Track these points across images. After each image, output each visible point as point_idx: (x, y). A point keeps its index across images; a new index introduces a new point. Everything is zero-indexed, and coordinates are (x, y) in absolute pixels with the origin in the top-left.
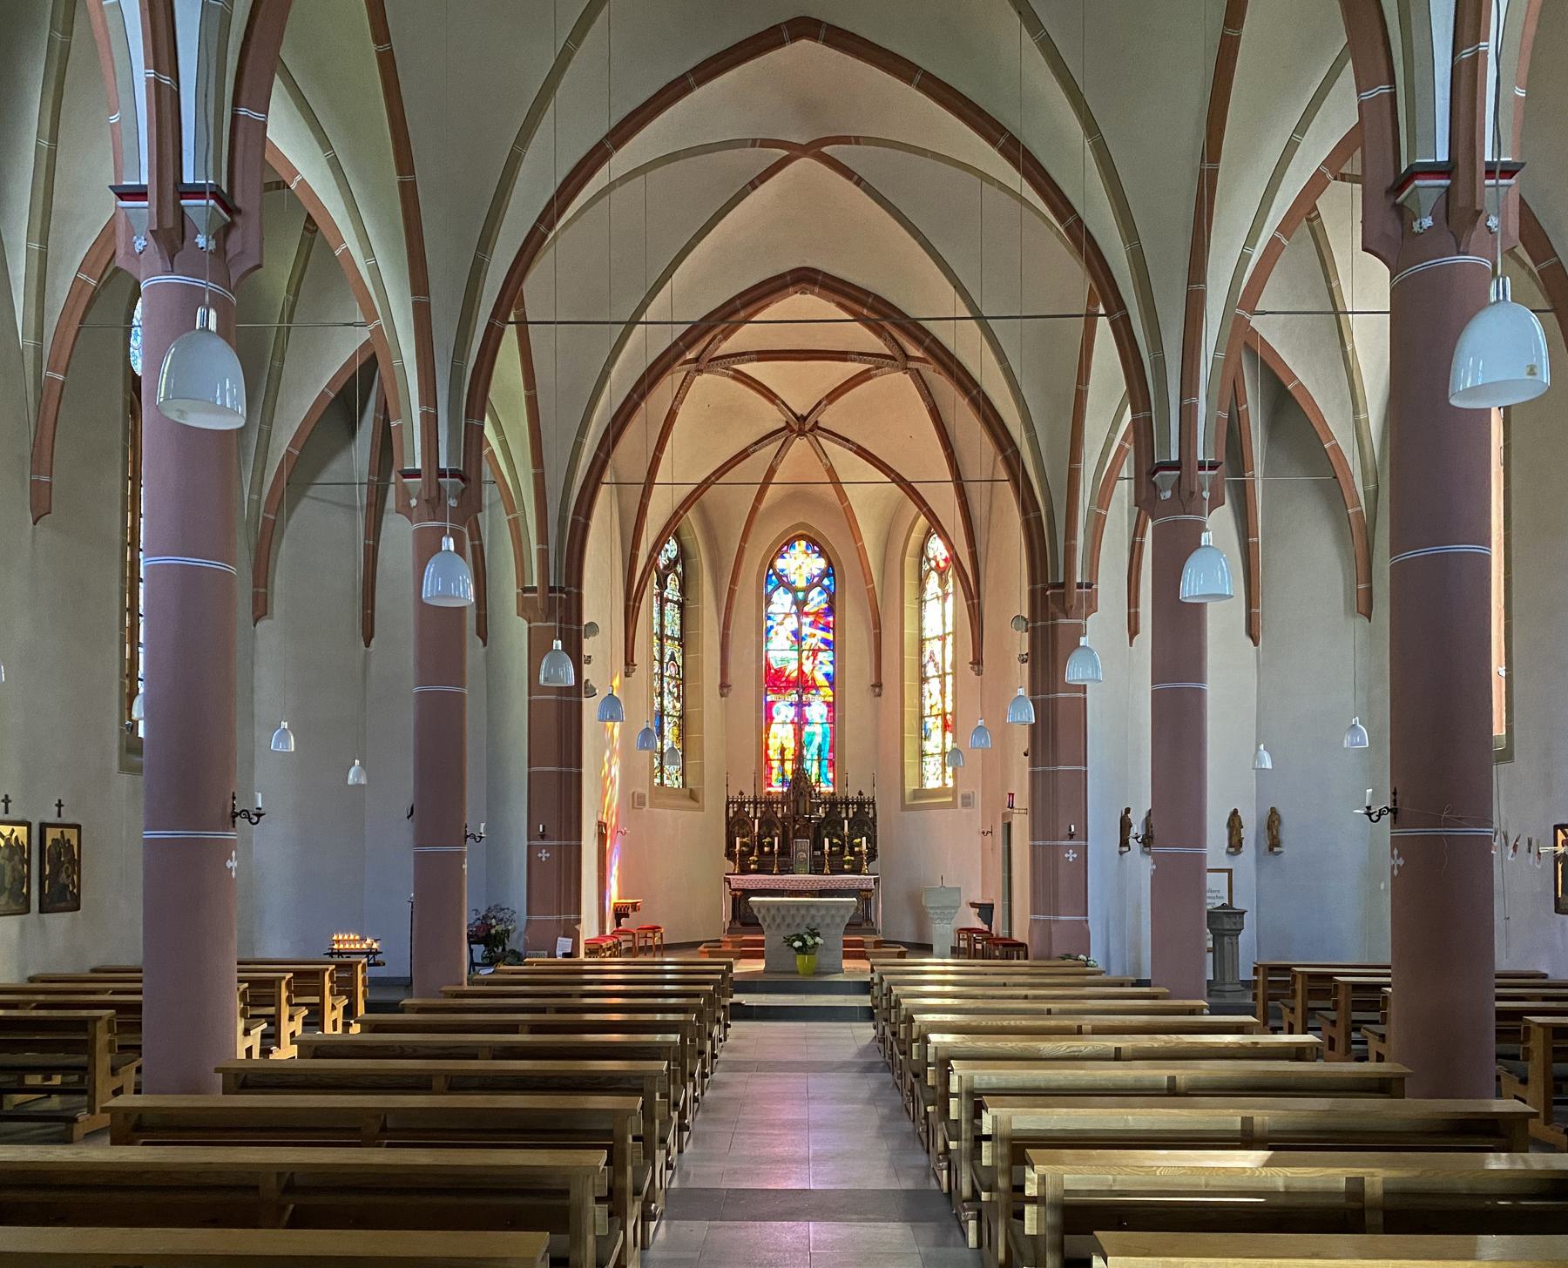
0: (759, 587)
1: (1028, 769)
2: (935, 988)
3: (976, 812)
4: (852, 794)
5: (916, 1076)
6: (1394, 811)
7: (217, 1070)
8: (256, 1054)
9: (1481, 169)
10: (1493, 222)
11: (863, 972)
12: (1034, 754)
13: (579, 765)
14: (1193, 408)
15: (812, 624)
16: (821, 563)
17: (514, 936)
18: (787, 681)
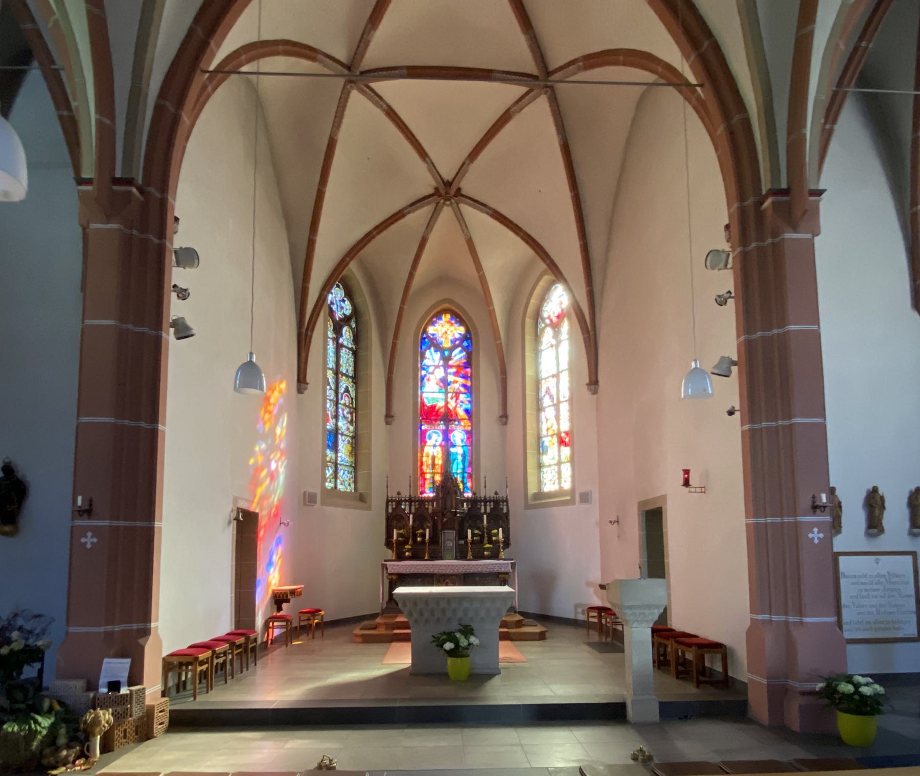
4: (490, 494)
15: (456, 374)
16: (462, 330)
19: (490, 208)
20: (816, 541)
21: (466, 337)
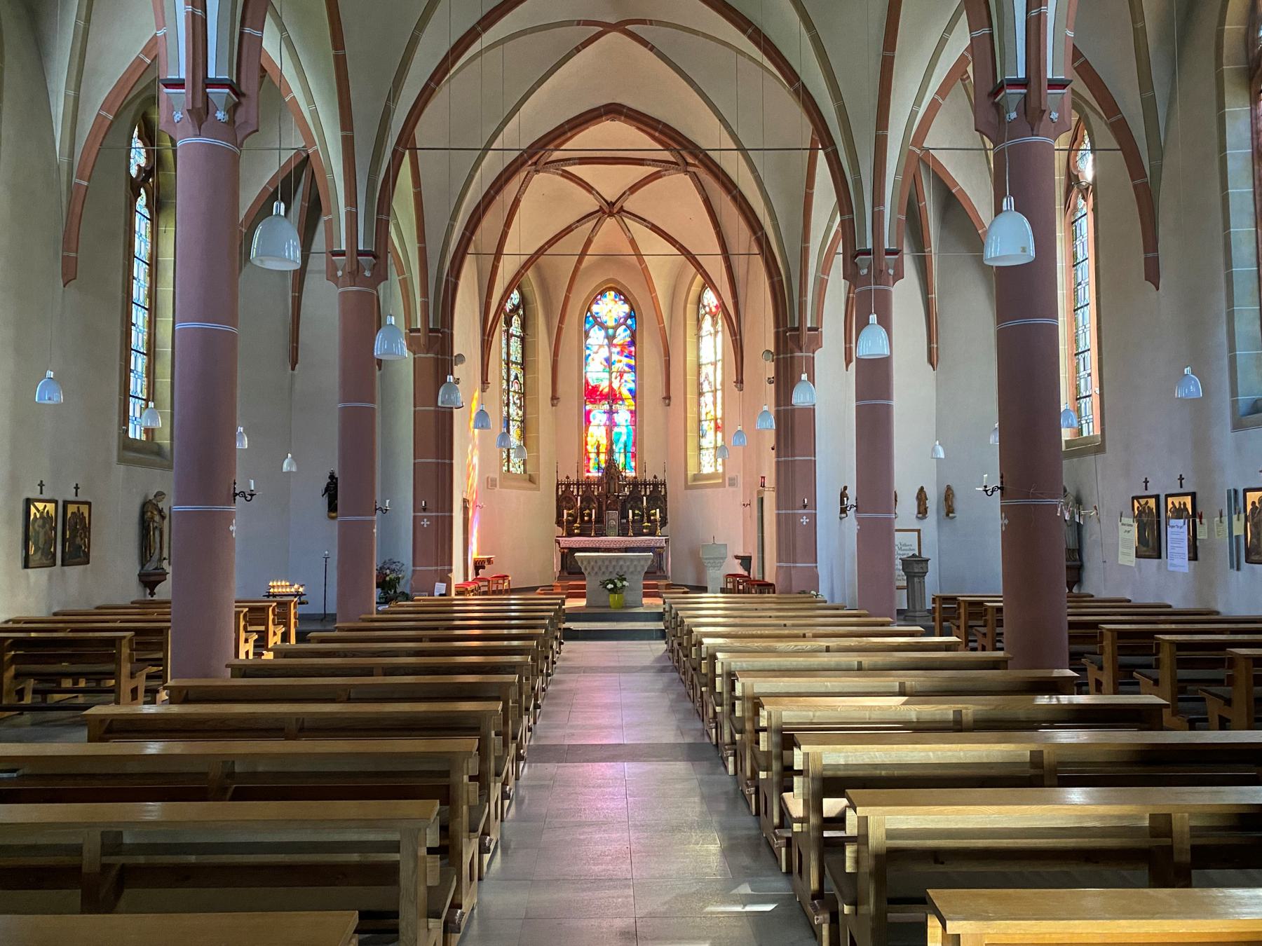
0: (580, 326)
1: (774, 460)
2: (709, 614)
3: (739, 489)
4: (649, 478)
5: (694, 669)
6: (1001, 488)
7: (227, 666)
8: (251, 656)
9: (1045, 84)
10: (1054, 116)
11: (658, 606)
12: (778, 448)
13: (451, 458)
14: (881, 213)
16: (626, 308)
17: (402, 582)
18: (601, 394)
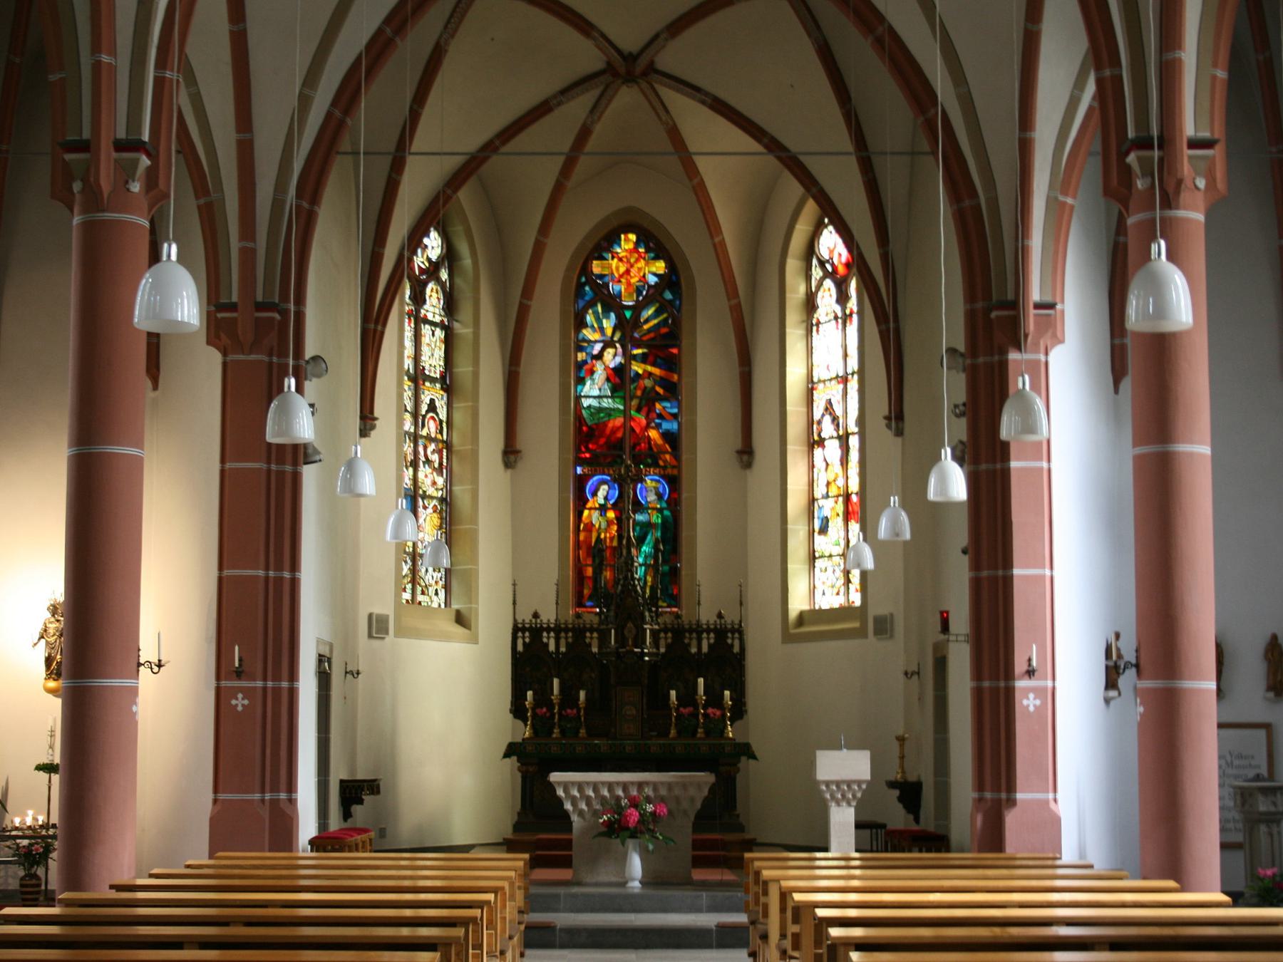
19: (707, 94)
20: (240, 708)
21: (670, 281)
